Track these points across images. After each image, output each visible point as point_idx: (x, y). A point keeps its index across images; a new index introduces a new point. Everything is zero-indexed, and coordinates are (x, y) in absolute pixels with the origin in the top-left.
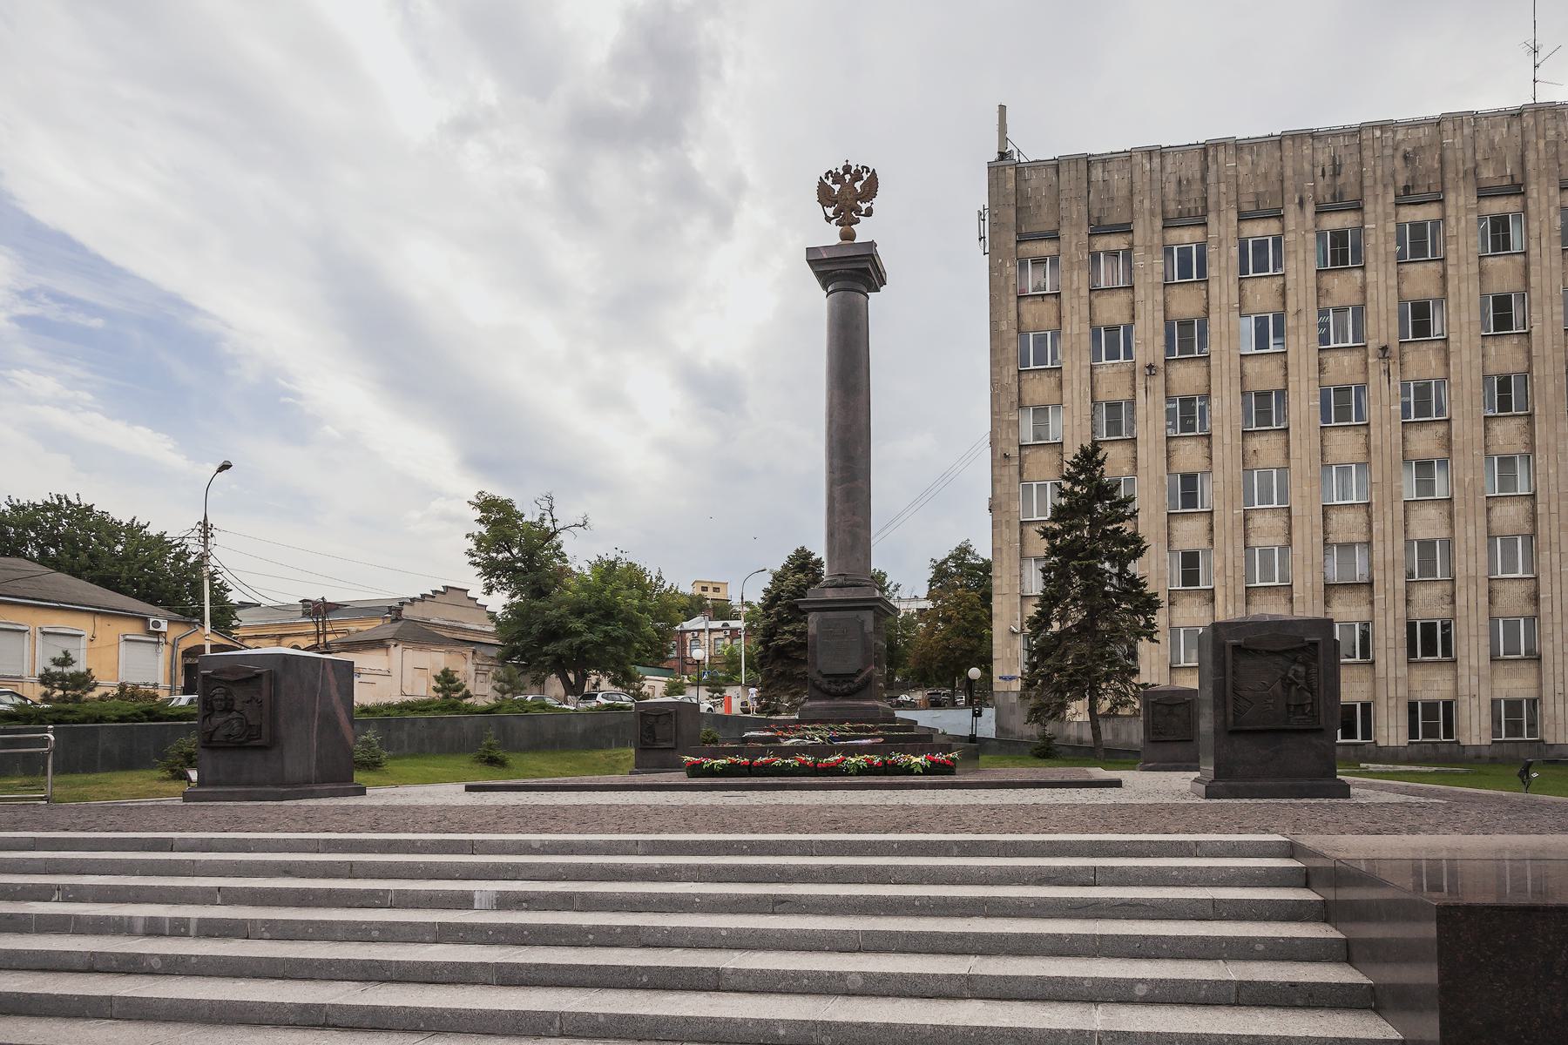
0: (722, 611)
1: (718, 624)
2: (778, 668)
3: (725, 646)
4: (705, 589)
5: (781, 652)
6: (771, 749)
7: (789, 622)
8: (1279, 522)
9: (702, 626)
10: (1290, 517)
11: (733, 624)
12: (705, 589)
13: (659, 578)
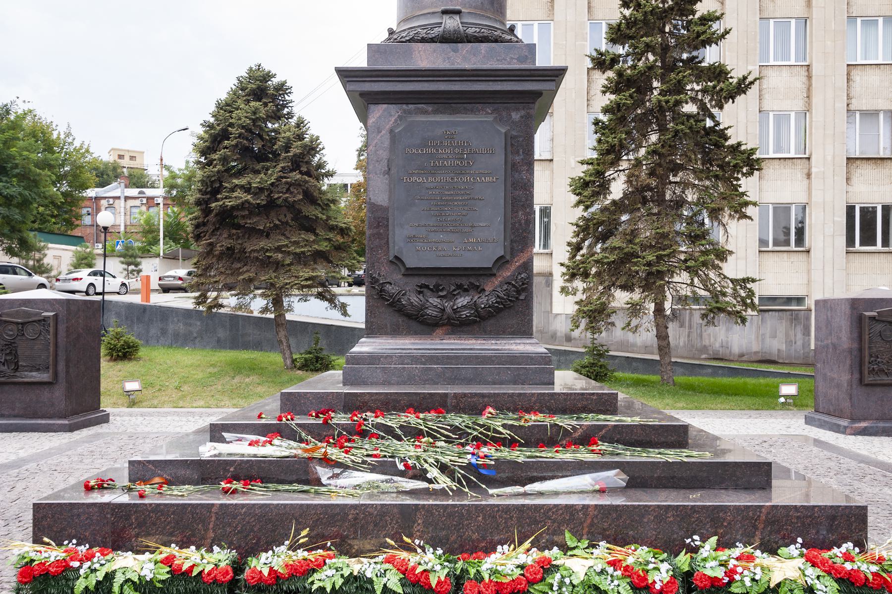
0: (138, 180)
1: (134, 192)
2: (223, 242)
3: (141, 213)
4: (121, 157)
5: (227, 217)
6: (301, 515)
7: (239, 174)
8: (798, 81)
9: (117, 193)
10: (809, 77)
11: (149, 192)
12: (121, 157)
13: (68, 135)
